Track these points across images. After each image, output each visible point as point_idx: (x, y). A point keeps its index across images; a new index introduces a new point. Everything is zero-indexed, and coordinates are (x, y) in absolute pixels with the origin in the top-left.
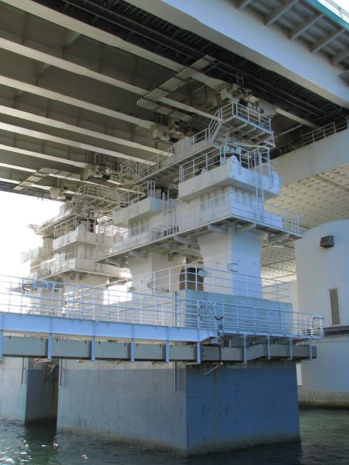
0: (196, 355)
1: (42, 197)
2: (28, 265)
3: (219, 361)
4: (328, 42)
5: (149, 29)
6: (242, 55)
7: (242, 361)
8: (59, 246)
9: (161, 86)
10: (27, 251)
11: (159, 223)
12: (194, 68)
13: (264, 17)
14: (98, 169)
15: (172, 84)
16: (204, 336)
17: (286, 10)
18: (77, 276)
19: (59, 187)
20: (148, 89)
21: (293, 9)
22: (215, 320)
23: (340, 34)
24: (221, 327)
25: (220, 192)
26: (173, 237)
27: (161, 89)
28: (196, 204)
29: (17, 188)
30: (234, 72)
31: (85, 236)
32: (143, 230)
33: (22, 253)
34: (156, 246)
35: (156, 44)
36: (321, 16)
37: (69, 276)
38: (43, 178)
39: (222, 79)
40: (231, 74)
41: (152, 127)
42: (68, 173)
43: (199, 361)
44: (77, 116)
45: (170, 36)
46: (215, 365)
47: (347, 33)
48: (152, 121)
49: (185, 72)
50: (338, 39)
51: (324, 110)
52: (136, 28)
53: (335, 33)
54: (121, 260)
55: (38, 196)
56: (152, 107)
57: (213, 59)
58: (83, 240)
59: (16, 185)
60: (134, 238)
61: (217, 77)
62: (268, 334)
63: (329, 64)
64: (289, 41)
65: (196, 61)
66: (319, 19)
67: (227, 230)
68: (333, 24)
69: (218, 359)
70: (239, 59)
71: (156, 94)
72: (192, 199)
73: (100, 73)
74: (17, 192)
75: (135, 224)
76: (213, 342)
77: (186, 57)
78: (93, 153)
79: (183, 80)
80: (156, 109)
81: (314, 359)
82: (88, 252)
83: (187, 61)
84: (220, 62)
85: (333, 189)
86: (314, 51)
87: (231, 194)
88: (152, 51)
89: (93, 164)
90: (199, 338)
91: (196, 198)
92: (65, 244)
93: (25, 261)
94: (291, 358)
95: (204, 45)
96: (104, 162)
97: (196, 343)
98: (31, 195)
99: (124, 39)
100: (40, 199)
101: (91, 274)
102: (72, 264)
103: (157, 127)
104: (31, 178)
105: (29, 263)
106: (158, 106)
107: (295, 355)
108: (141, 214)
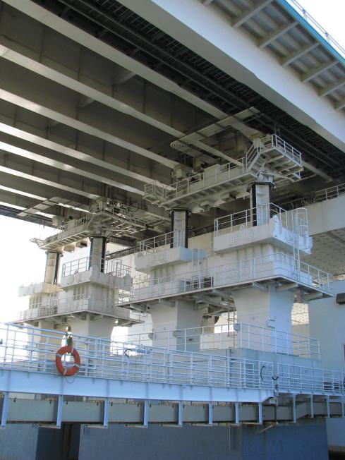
0: (258, 416)
1: (44, 224)
2: (26, 300)
3: (274, 421)
4: (335, 88)
5: (194, 70)
6: (284, 109)
7: (292, 420)
8: (68, 284)
9: (199, 131)
10: (27, 285)
11: (186, 273)
12: (236, 118)
13: (231, 17)
14: (110, 202)
15: (210, 130)
16: (264, 397)
17: (256, 12)
18: (88, 316)
19: (64, 216)
20: (185, 132)
21: (264, 10)
22: (272, 380)
23: (333, 65)
24: (277, 387)
25: (258, 250)
26: (211, 290)
27: (200, 134)
28: (229, 259)
29: (20, 214)
30: (272, 124)
31: (99, 277)
32: (168, 280)
33: (21, 287)
34: (182, 298)
35: (186, 79)
36: (295, 24)
37: (80, 317)
38: (52, 207)
39: (260, 129)
40: (268, 125)
41: (176, 166)
42: (66, 200)
43: (261, 421)
44: (103, 149)
45: (149, 39)
46: (270, 425)
47: (340, 65)
48: (177, 161)
49: (227, 120)
50: (329, 71)
51: (340, 163)
52: (142, 44)
53: (308, 45)
54: (143, 306)
55: (40, 223)
56: (183, 149)
57: (257, 111)
58: (96, 280)
59: (21, 211)
60: (158, 287)
61: (252, 127)
62: (310, 393)
63: (278, 65)
64: (318, 98)
65: (240, 111)
66: (292, 26)
67: (268, 287)
68: (325, 54)
69: (273, 418)
70: (299, 125)
71: (193, 138)
72: (227, 253)
73: (79, 81)
74: (19, 218)
75: (159, 271)
76: (271, 402)
77: (231, 106)
78: (105, 185)
79: (224, 128)
80: (186, 151)
81: (336, 420)
82: (105, 293)
83: (230, 109)
84: (263, 114)
85: (339, 245)
86: (322, 96)
87: (270, 254)
88: (202, 98)
89: (104, 196)
90: (260, 399)
91: (231, 252)
92: (75, 283)
93: (25, 295)
94: (313, 417)
95: (252, 97)
96: (116, 195)
97: (256, 404)
98: (32, 221)
99: (180, 85)
100: (42, 226)
101: (104, 316)
102: (83, 305)
103: (181, 168)
104: (39, 206)
105: (28, 298)
106: (190, 148)
107: (316, 413)
108: (168, 262)
